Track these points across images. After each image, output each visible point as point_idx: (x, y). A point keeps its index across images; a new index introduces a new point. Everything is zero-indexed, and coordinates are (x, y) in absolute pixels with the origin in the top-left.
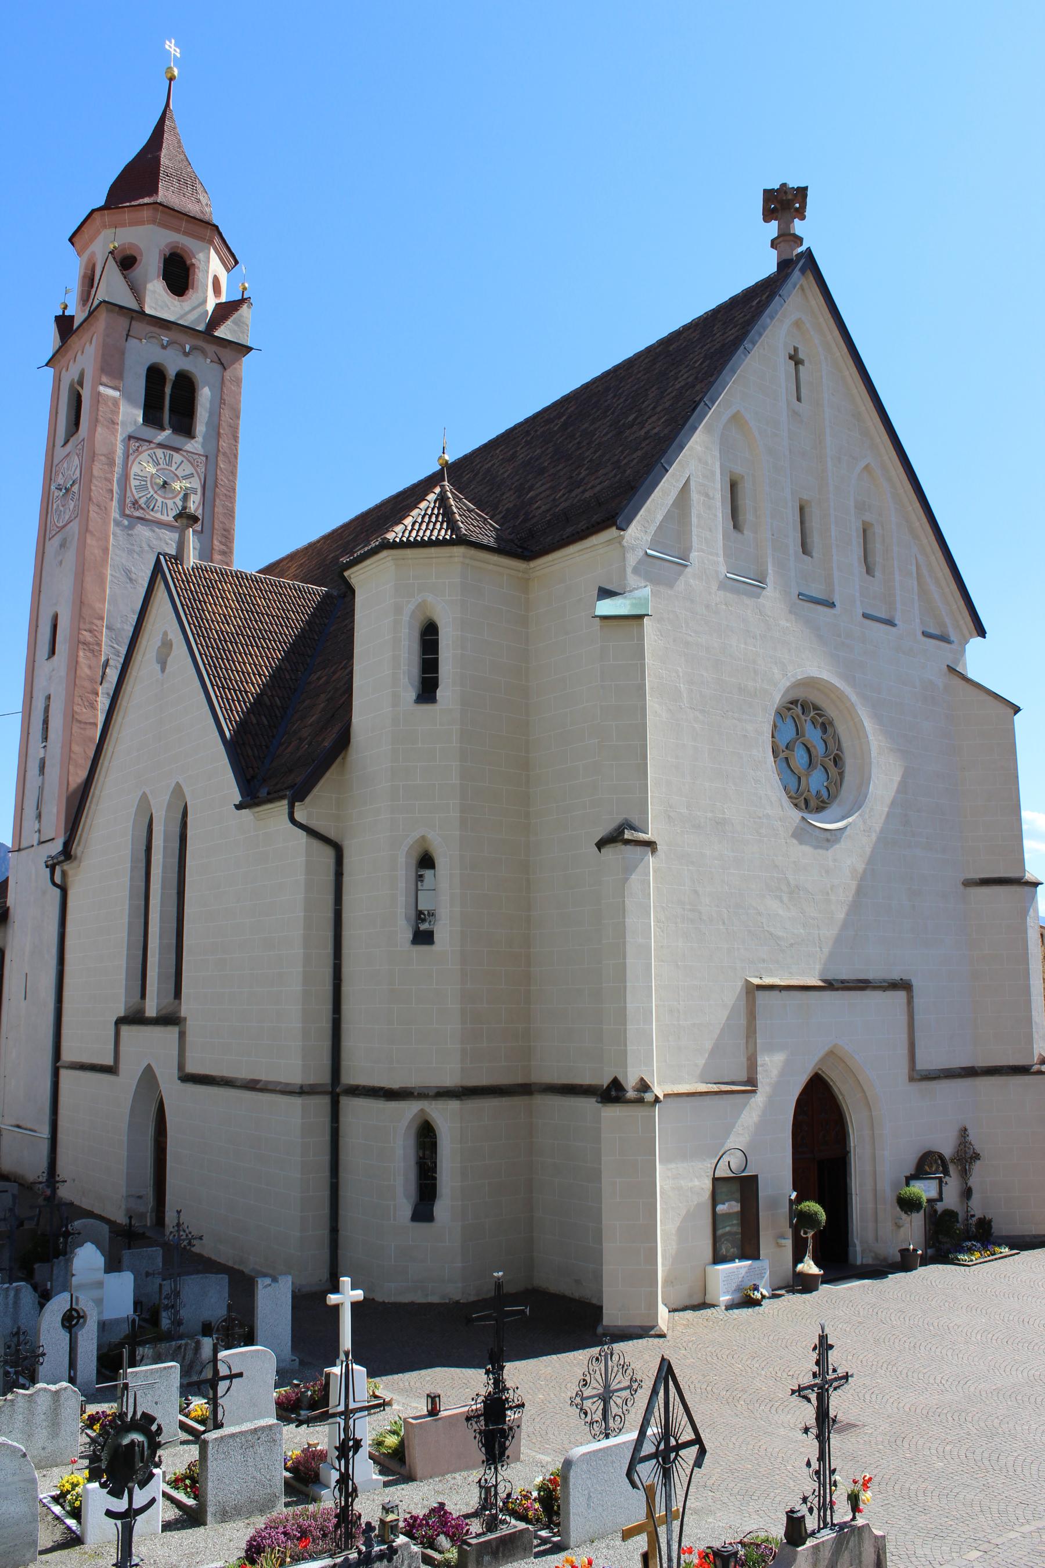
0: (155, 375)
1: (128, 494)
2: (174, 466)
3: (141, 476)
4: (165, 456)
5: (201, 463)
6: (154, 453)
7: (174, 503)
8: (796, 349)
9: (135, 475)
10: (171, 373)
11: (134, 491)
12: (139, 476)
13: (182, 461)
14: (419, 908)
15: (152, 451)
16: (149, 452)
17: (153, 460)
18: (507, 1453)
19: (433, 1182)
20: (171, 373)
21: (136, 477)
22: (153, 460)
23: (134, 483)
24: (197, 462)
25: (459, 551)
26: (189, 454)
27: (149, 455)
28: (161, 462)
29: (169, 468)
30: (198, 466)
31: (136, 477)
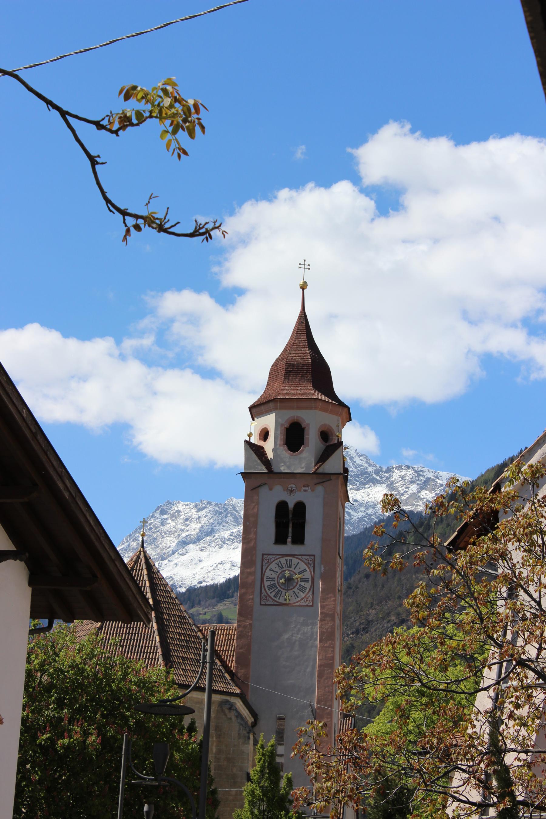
0: (282, 507)
1: (263, 591)
2: (293, 567)
3: (271, 578)
4: (287, 562)
5: (311, 561)
6: (280, 561)
7: (293, 591)
8: (216, 221)
9: (267, 578)
10: (291, 506)
11: (267, 589)
12: (270, 578)
13: (299, 563)
14: (345, 467)
15: (278, 560)
16: (276, 561)
17: (279, 566)
18: (537, 439)
19: (289, 539)
20: (291, 506)
21: (268, 579)
22: (279, 566)
23: (267, 584)
24: (308, 561)
25: (65, 109)
26: (303, 557)
27: (276, 563)
28: (284, 566)
29: (297, 587)
30: (309, 563)
31: (268, 579)
